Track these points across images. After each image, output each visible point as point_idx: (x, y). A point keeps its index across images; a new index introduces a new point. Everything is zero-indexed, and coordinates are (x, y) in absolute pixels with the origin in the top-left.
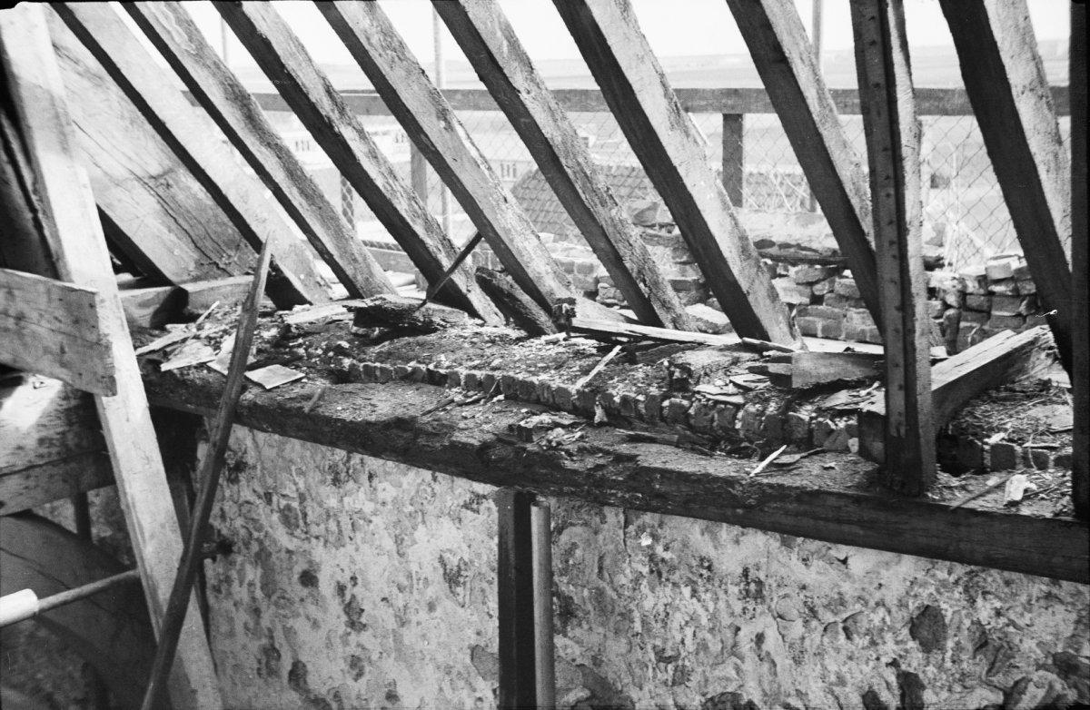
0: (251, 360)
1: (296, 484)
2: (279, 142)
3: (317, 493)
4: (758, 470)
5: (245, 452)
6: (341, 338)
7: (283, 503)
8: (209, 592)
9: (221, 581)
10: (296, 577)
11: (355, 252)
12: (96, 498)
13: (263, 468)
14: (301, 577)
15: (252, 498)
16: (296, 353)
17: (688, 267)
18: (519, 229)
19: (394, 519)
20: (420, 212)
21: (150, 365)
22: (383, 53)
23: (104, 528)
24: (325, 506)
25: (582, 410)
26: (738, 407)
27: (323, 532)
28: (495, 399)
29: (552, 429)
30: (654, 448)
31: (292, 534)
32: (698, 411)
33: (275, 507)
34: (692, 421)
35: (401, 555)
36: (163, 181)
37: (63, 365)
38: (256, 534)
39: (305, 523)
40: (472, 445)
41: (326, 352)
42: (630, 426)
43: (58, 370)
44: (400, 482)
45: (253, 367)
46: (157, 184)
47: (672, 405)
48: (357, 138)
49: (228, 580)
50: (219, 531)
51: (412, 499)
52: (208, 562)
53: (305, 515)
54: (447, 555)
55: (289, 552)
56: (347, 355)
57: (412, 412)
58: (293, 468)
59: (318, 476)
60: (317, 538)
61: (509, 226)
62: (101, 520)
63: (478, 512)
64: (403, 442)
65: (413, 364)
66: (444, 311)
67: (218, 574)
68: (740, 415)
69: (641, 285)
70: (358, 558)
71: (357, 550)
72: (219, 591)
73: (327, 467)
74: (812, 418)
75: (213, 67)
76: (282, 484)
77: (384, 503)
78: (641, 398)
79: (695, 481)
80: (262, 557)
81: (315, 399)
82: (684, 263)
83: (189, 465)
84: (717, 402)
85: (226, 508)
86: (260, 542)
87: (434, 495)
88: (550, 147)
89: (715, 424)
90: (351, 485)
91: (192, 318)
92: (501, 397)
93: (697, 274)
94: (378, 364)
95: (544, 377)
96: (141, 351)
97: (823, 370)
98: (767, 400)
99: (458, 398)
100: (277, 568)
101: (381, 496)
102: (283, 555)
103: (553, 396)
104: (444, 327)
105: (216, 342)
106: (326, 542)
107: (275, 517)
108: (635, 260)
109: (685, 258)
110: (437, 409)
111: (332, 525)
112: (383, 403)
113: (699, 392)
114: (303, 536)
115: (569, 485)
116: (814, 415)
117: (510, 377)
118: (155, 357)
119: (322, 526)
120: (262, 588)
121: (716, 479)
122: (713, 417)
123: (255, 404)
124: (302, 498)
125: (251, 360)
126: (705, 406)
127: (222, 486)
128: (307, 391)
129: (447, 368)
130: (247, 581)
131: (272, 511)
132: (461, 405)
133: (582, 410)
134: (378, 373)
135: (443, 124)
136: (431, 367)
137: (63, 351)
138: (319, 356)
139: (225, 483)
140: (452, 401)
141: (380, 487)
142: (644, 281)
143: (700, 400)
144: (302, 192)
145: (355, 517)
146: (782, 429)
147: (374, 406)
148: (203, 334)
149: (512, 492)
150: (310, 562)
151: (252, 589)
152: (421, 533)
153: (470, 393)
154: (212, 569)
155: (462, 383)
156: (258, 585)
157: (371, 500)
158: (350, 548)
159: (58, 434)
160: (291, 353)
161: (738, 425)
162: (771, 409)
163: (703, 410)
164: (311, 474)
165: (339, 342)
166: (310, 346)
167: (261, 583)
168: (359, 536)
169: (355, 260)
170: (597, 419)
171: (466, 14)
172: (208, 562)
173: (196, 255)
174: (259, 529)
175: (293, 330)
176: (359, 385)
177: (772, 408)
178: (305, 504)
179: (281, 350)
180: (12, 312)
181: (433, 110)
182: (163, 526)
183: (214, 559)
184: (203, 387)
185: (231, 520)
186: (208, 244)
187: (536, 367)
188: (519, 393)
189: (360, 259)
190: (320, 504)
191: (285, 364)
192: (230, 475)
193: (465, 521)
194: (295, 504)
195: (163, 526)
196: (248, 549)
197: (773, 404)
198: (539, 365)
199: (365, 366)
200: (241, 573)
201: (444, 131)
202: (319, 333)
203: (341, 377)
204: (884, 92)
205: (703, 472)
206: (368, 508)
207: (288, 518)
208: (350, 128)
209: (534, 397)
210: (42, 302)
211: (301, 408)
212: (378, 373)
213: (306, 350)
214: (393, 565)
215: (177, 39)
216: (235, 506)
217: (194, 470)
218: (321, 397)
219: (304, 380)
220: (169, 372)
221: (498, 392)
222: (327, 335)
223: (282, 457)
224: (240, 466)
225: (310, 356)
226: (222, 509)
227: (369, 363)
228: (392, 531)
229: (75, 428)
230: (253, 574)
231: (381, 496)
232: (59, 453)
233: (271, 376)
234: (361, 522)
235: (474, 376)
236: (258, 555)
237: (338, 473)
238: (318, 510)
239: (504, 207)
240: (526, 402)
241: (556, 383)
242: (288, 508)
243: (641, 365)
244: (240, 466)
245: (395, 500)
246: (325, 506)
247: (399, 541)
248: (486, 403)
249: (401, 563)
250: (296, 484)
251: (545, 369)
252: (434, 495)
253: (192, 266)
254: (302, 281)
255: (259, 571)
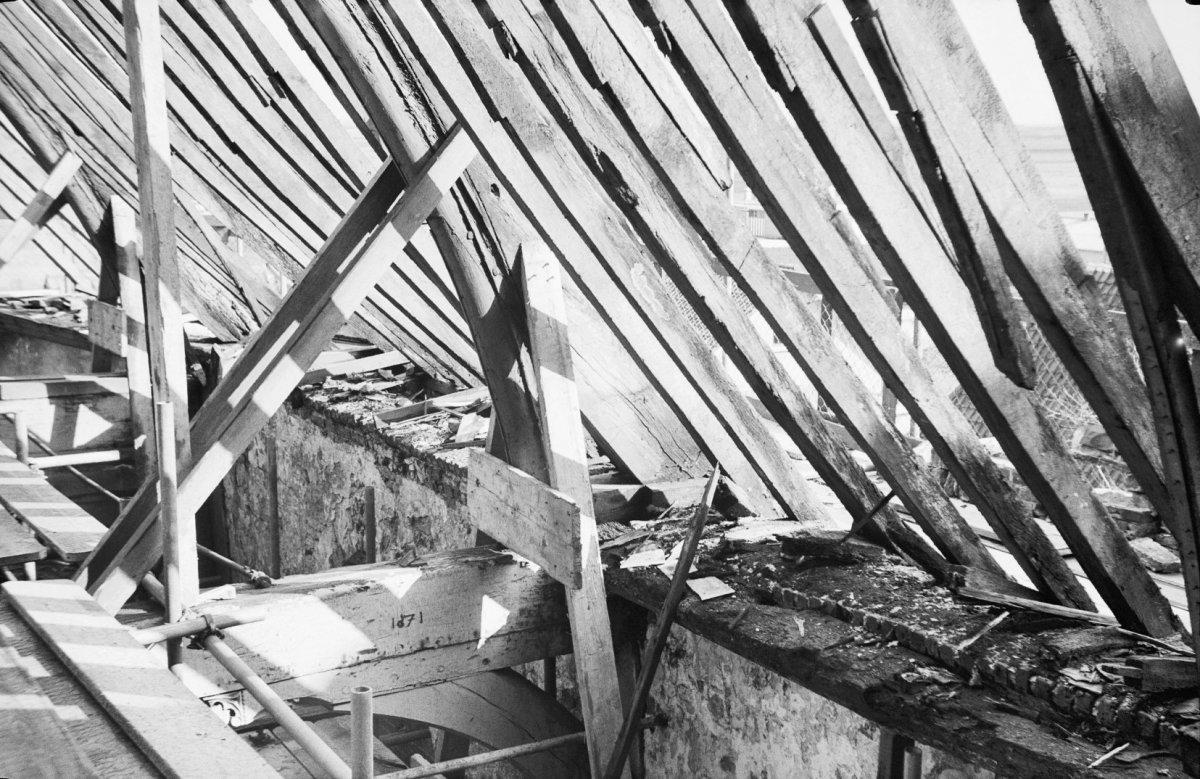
0: (693, 569)
1: (724, 679)
2: (732, 388)
3: (740, 690)
4: (1096, 763)
5: (685, 642)
6: (770, 561)
7: (712, 693)
8: (646, 756)
9: (656, 750)
10: (718, 760)
11: (793, 480)
12: (561, 662)
13: (698, 659)
14: (722, 761)
15: (688, 683)
16: (731, 567)
17: (1141, 498)
18: (928, 492)
19: (802, 727)
20: (847, 461)
21: (612, 557)
22: (812, 352)
23: (568, 681)
24: (746, 703)
25: (960, 669)
26: (1096, 696)
27: (742, 726)
28: (890, 644)
29: (929, 684)
30: (1015, 721)
31: (717, 722)
32: (1061, 691)
33: (705, 694)
34: (1055, 700)
35: (805, 761)
36: (640, 396)
37: (544, 555)
38: (688, 715)
39: (729, 715)
40: (860, 687)
41: (756, 571)
42: (996, 695)
43: (539, 558)
44: (805, 701)
45: (694, 576)
46: (632, 400)
47: (1038, 682)
48: (794, 400)
49: (662, 750)
50: (658, 705)
51: (817, 714)
52: (647, 731)
53: (729, 708)
54: (843, 770)
55: (713, 736)
56: (773, 579)
57: (817, 645)
58: (723, 664)
59: (742, 676)
60: (737, 730)
61: (919, 489)
62: (566, 674)
63: (872, 739)
64: (802, 667)
65: (825, 597)
66: (863, 547)
67: (655, 743)
68: (1097, 703)
69: (1033, 560)
70: (769, 755)
71: (769, 747)
72: (654, 757)
73: (750, 670)
74: (1160, 721)
75: (682, 330)
76: (712, 676)
77: (794, 712)
78: (1012, 670)
79: (1043, 761)
80: (691, 736)
81: (739, 617)
82: (1138, 493)
83: (639, 642)
84: (1077, 688)
85: (666, 687)
86: (691, 724)
87: (836, 714)
88: (946, 444)
89: (1075, 707)
90: (768, 690)
91: (654, 516)
92: (895, 643)
93: (1149, 507)
94: (796, 592)
95: (932, 632)
96: (603, 547)
97: (1178, 677)
98: (1124, 695)
99: (858, 638)
100: (703, 749)
101: (793, 705)
102: (708, 738)
103: (939, 652)
104: (863, 561)
105: (669, 546)
106: (744, 735)
107: (705, 704)
108: (1027, 537)
109: (1139, 489)
110: (837, 646)
111: (751, 723)
112: (798, 629)
113: (1063, 675)
114: (726, 726)
115: (938, 739)
116: (1162, 717)
117: (904, 627)
118: (616, 552)
119: (743, 720)
120: (689, 763)
121: (1058, 764)
122: (1073, 701)
123: (691, 612)
124: (728, 692)
125: (693, 569)
126: (1066, 689)
127: (663, 667)
128: (733, 607)
129: (854, 606)
130: (677, 755)
131: (703, 698)
132: (860, 645)
133: (960, 669)
134: (796, 599)
135: (862, 405)
136: (840, 603)
137: (544, 545)
138: (750, 574)
139: (667, 665)
140: (852, 640)
141: (792, 697)
142: (1036, 557)
143: (1063, 683)
144: (750, 430)
145: (769, 718)
146: (1133, 725)
147: (786, 632)
148: (660, 535)
149: (892, 733)
150: (730, 749)
151: (681, 762)
152: (822, 745)
153: (870, 635)
154: (650, 739)
155: (865, 623)
156: (686, 760)
157: (784, 707)
158: (763, 745)
159: (535, 606)
160: (728, 567)
161: (1095, 713)
162: (1125, 704)
163: (1065, 692)
164: (737, 672)
165: (767, 566)
166: (744, 564)
167: (689, 758)
168: (772, 735)
169: (793, 488)
170: (972, 682)
171: (872, 343)
172: (647, 731)
173: (663, 459)
174: (691, 711)
175: (732, 547)
176: (778, 609)
177: (1126, 704)
178: (730, 698)
179: (718, 563)
180: (511, 503)
181: (854, 395)
182: (608, 702)
183: (652, 731)
184: (651, 588)
185: (669, 698)
186: (675, 449)
187: (929, 620)
188: (914, 645)
189: (797, 487)
190: (742, 701)
191: (721, 577)
192: (671, 659)
193: (860, 744)
194: (722, 696)
195: (608, 702)
196: (681, 726)
197: (1127, 700)
198: (933, 619)
199: (786, 592)
200: (673, 744)
201: (861, 411)
202: (753, 552)
203: (767, 599)
204: (1184, 489)
205: (1049, 754)
206: (781, 713)
207: (715, 707)
208: (789, 392)
209: (923, 649)
210: (533, 501)
211: (728, 623)
212: (796, 599)
213: (740, 567)
214: (798, 769)
215: (655, 309)
216: (675, 684)
217: (643, 648)
218: (745, 616)
219: (734, 596)
220: (626, 569)
221: (894, 638)
222: (758, 555)
223: (714, 653)
224: (680, 653)
225: (743, 573)
226: (662, 686)
227: (790, 589)
228: (799, 737)
229: (550, 602)
230: (683, 749)
231: (793, 705)
232: (534, 623)
233: (709, 588)
234: (774, 724)
235: (875, 619)
236: (688, 734)
237: (758, 677)
238: (740, 706)
239: (914, 473)
240: (916, 652)
241: (943, 640)
242: (716, 697)
243: (1020, 636)
244: (680, 653)
245: (803, 711)
246: (746, 703)
247: (804, 748)
248: (880, 647)
249: (804, 768)
250: (724, 679)
251: (935, 625)
252: (836, 714)
253: (658, 468)
254: (750, 494)
255: (688, 749)
